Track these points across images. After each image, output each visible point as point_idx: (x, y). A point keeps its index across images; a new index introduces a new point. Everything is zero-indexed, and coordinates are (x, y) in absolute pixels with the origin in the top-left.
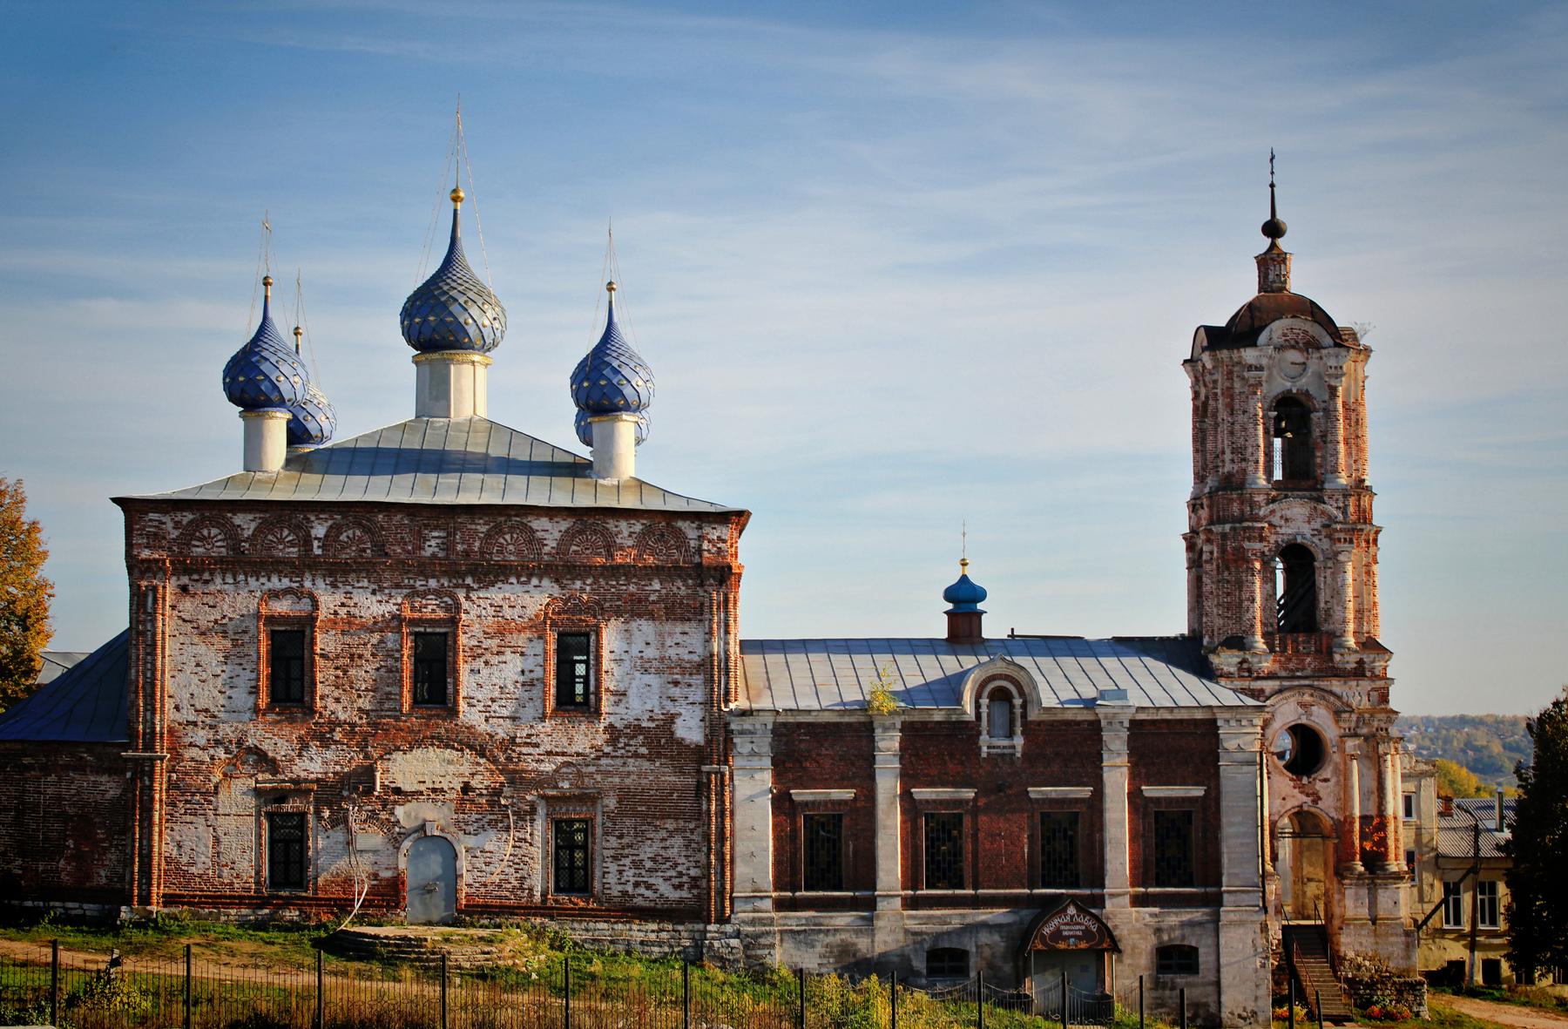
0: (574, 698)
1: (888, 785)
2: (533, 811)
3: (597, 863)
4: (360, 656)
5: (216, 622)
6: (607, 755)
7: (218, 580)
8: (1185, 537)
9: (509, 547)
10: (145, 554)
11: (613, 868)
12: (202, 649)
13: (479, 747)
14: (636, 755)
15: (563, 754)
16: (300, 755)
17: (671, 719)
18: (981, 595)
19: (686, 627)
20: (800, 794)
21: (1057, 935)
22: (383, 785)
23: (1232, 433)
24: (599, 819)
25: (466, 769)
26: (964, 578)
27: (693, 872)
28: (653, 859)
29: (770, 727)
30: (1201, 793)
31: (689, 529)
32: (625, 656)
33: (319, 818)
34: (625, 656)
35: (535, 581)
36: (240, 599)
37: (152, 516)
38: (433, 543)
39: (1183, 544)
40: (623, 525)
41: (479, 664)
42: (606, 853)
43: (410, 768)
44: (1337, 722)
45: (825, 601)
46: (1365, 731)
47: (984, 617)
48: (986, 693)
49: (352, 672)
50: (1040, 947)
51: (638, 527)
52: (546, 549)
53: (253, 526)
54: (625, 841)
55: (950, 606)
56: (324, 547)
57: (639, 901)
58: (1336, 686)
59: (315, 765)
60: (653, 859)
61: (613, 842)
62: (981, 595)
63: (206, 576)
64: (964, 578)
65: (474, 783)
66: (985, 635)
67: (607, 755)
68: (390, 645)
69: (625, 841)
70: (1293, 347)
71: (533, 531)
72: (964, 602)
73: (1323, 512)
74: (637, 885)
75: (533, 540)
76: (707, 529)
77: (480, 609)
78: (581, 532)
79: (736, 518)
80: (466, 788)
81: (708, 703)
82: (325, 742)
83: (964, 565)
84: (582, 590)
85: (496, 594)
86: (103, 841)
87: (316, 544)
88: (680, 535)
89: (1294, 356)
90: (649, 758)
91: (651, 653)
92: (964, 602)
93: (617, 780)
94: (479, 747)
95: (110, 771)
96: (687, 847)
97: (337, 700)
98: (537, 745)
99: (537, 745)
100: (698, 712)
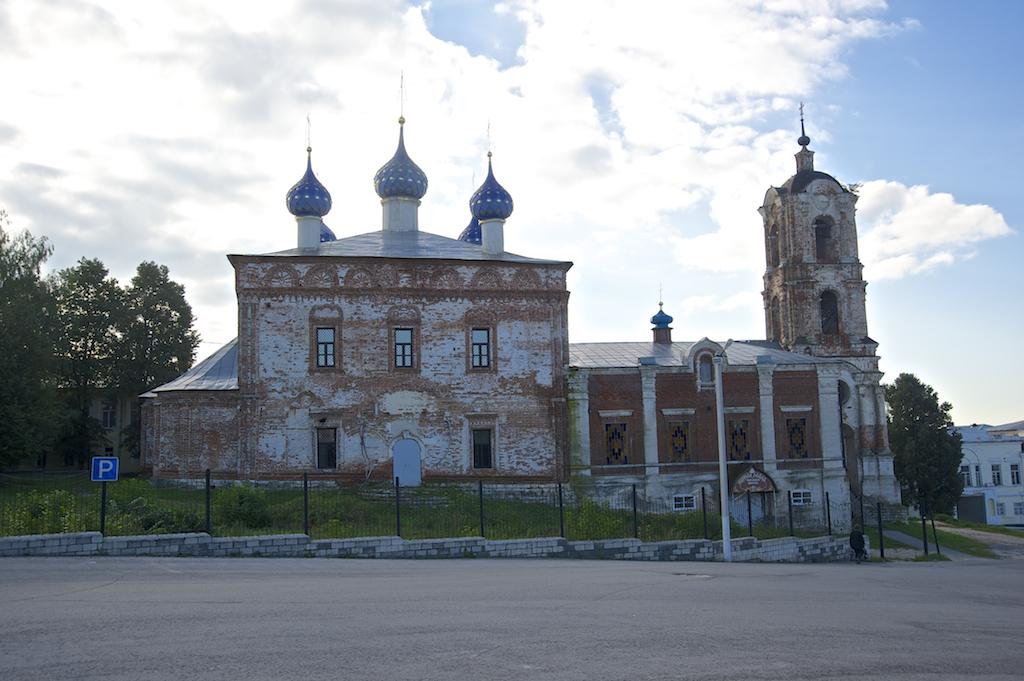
0: (484, 365)
1: (767, 402)
2: (461, 424)
3: (497, 451)
4: (365, 341)
5: (286, 323)
6: (500, 393)
7: (287, 300)
8: (763, 294)
9: (445, 282)
10: (247, 285)
11: (505, 454)
12: (278, 337)
13: (431, 390)
14: (516, 393)
15: (477, 393)
16: (333, 396)
17: (534, 373)
18: (670, 320)
19: (541, 324)
20: (604, 414)
21: (745, 484)
22: (379, 411)
23: (794, 236)
24: (497, 429)
25: (425, 401)
26: (661, 312)
27: (548, 456)
28: (526, 449)
29: (587, 376)
30: (810, 409)
31: (541, 273)
32: (509, 341)
33: (345, 431)
34: (509, 341)
35: (460, 300)
36: (299, 309)
37: (250, 265)
38: (404, 280)
39: (762, 297)
40: (506, 270)
41: (430, 345)
42: (502, 446)
43: (397, 401)
44: (853, 378)
45: (602, 323)
46: (867, 382)
47: (672, 331)
48: (699, 358)
49: (361, 350)
50: (737, 491)
51: (514, 272)
52: (466, 283)
53: (306, 270)
54: (511, 440)
55: (654, 326)
56: (345, 282)
57: (519, 473)
58: (852, 360)
59: (342, 400)
60: (526, 449)
61: (505, 440)
62: (670, 320)
63: (281, 298)
64: (661, 312)
65: (430, 410)
66: (673, 340)
67: (500, 393)
68: (382, 335)
69: (511, 440)
70: (823, 194)
71: (458, 274)
72: (662, 323)
73: (841, 275)
74: (518, 463)
75: (458, 278)
76: (551, 272)
77: (434, 313)
78: (484, 274)
79: (569, 265)
80: (425, 412)
81: (555, 364)
82: (347, 389)
83: (661, 304)
84: (485, 305)
85: (439, 307)
86: (225, 444)
87: (341, 280)
88: (536, 276)
89: (823, 198)
90: (523, 395)
91: (523, 338)
92: (662, 323)
93: (506, 407)
94: (431, 390)
95: (227, 406)
96: (545, 442)
97: (353, 365)
98: (462, 389)
99: (462, 389)
100: (549, 370)
